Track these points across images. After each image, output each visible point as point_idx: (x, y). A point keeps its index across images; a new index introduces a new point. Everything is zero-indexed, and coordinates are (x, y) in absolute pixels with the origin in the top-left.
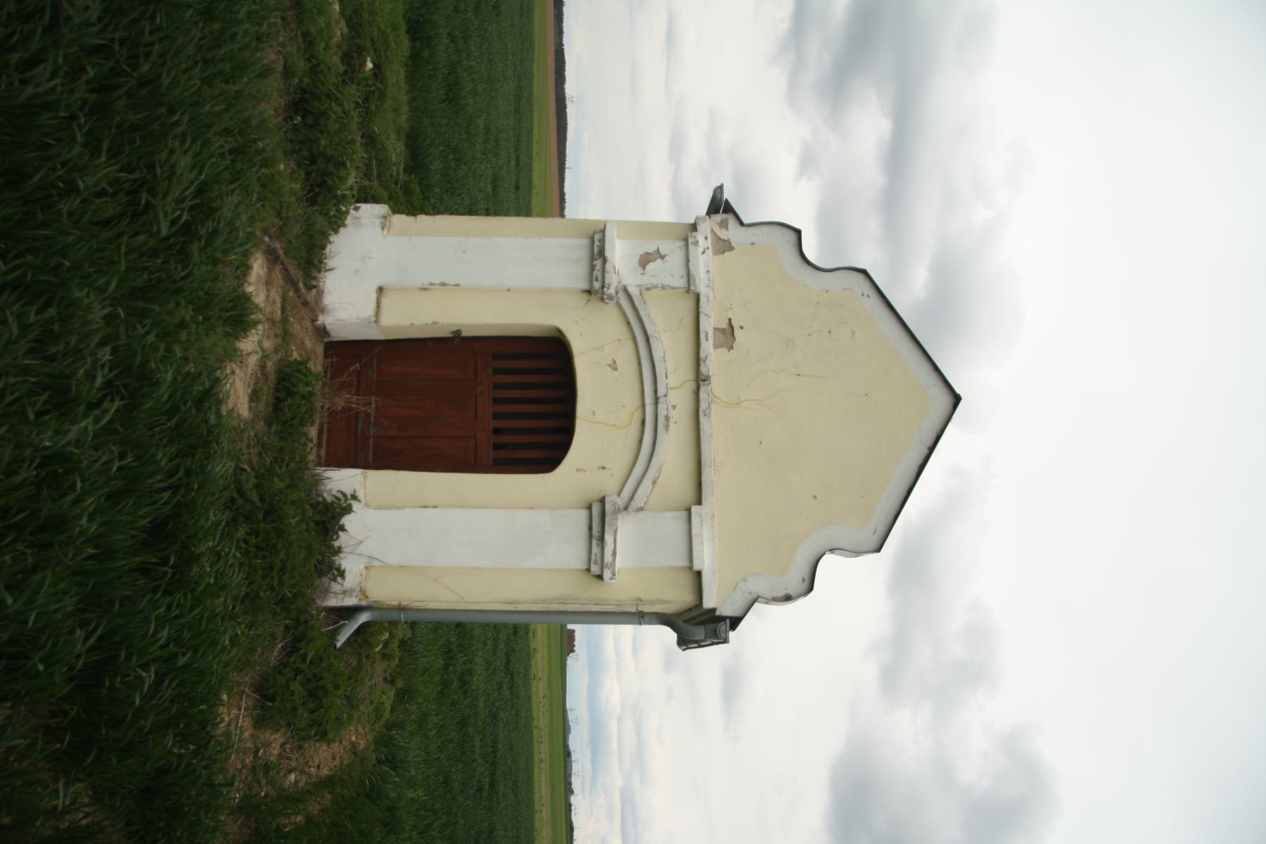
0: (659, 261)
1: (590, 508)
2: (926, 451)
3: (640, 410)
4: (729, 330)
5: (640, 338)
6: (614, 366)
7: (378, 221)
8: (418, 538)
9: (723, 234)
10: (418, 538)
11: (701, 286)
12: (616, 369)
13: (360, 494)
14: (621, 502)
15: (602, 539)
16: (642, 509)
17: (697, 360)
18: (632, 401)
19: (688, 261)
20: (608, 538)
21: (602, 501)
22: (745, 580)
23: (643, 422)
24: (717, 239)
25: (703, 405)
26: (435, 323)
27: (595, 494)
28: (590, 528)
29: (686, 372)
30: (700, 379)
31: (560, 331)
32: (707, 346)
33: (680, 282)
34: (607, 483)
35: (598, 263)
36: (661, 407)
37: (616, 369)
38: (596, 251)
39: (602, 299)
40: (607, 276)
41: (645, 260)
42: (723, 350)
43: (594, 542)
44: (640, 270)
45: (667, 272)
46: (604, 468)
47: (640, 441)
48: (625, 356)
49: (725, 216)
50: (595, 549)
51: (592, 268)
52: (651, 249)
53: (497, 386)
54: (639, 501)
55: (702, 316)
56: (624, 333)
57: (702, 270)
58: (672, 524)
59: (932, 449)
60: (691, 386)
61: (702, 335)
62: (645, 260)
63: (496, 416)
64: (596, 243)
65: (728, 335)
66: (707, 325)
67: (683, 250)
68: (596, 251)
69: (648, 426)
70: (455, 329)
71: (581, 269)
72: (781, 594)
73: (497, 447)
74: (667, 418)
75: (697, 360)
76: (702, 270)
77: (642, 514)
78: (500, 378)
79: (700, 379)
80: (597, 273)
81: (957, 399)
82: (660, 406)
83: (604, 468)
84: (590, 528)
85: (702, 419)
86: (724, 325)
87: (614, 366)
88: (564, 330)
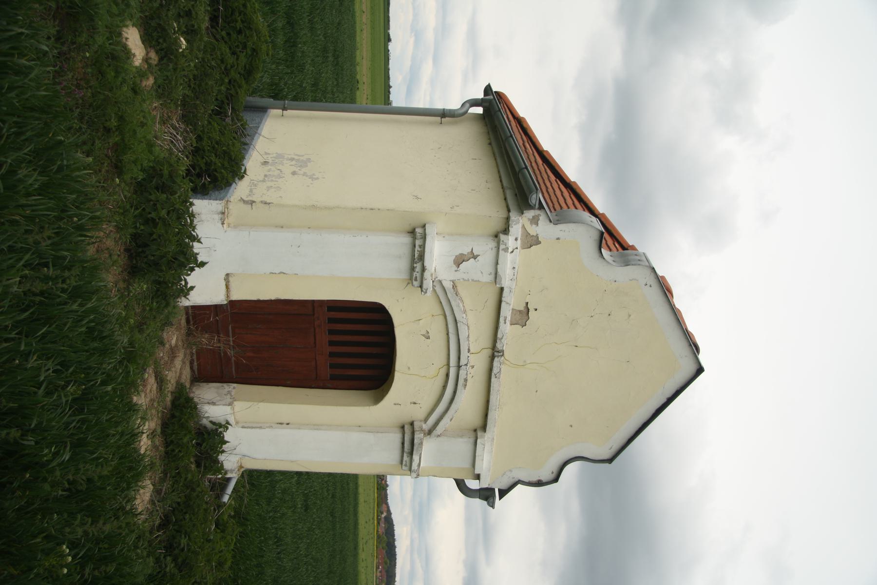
0: (472, 260)
1: (403, 427)
2: (664, 400)
3: (445, 368)
4: (526, 311)
5: (451, 324)
7: (217, 217)
8: (272, 432)
9: (532, 230)
10: (272, 432)
11: (506, 283)
12: (428, 338)
13: (232, 420)
14: (426, 427)
15: (411, 453)
16: (439, 436)
17: (495, 339)
18: (440, 360)
19: (497, 263)
20: (416, 457)
21: (412, 424)
22: (511, 471)
23: (447, 375)
24: (526, 234)
25: (495, 370)
27: (407, 419)
28: (403, 444)
29: (486, 342)
30: (495, 353)
32: (506, 328)
33: (488, 278)
34: (418, 413)
35: (418, 266)
36: (462, 373)
37: (428, 338)
38: (416, 255)
40: (425, 282)
41: (459, 261)
42: (534, 226)
43: (405, 455)
44: (455, 268)
45: (478, 270)
47: (445, 387)
48: (436, 328)
49: (537, 212)
50: (406, 458)
51: (413, 269)
52: (466, 251)
53: (331, 321)
54: (440, 429)
55: (503, 304)
56: (437, 310)
57: (509, 266)
58: (463, 445)
59: (670, 400)
60: (487, 352)
61: (502, 320)
62: (459, 261)
63: (331, 343)
64: (417, 248)
65: (523, 315)
66: (506, 312)
67: (495, 250)
68: (416, 255)
69: (451, 380)
71: (403, 264)
72: (534, 479)
73: (332, 366)
74: (466, 380)
75: (495, 339)
76: (509, 266)
77: (439, 439)
78: (333, 315)
79: (495, 353)
80: (417, 274)
81: (700, 370)
82: (461, 372)
84: (403, 444)
85: (493, 379)
86: (522, 307)
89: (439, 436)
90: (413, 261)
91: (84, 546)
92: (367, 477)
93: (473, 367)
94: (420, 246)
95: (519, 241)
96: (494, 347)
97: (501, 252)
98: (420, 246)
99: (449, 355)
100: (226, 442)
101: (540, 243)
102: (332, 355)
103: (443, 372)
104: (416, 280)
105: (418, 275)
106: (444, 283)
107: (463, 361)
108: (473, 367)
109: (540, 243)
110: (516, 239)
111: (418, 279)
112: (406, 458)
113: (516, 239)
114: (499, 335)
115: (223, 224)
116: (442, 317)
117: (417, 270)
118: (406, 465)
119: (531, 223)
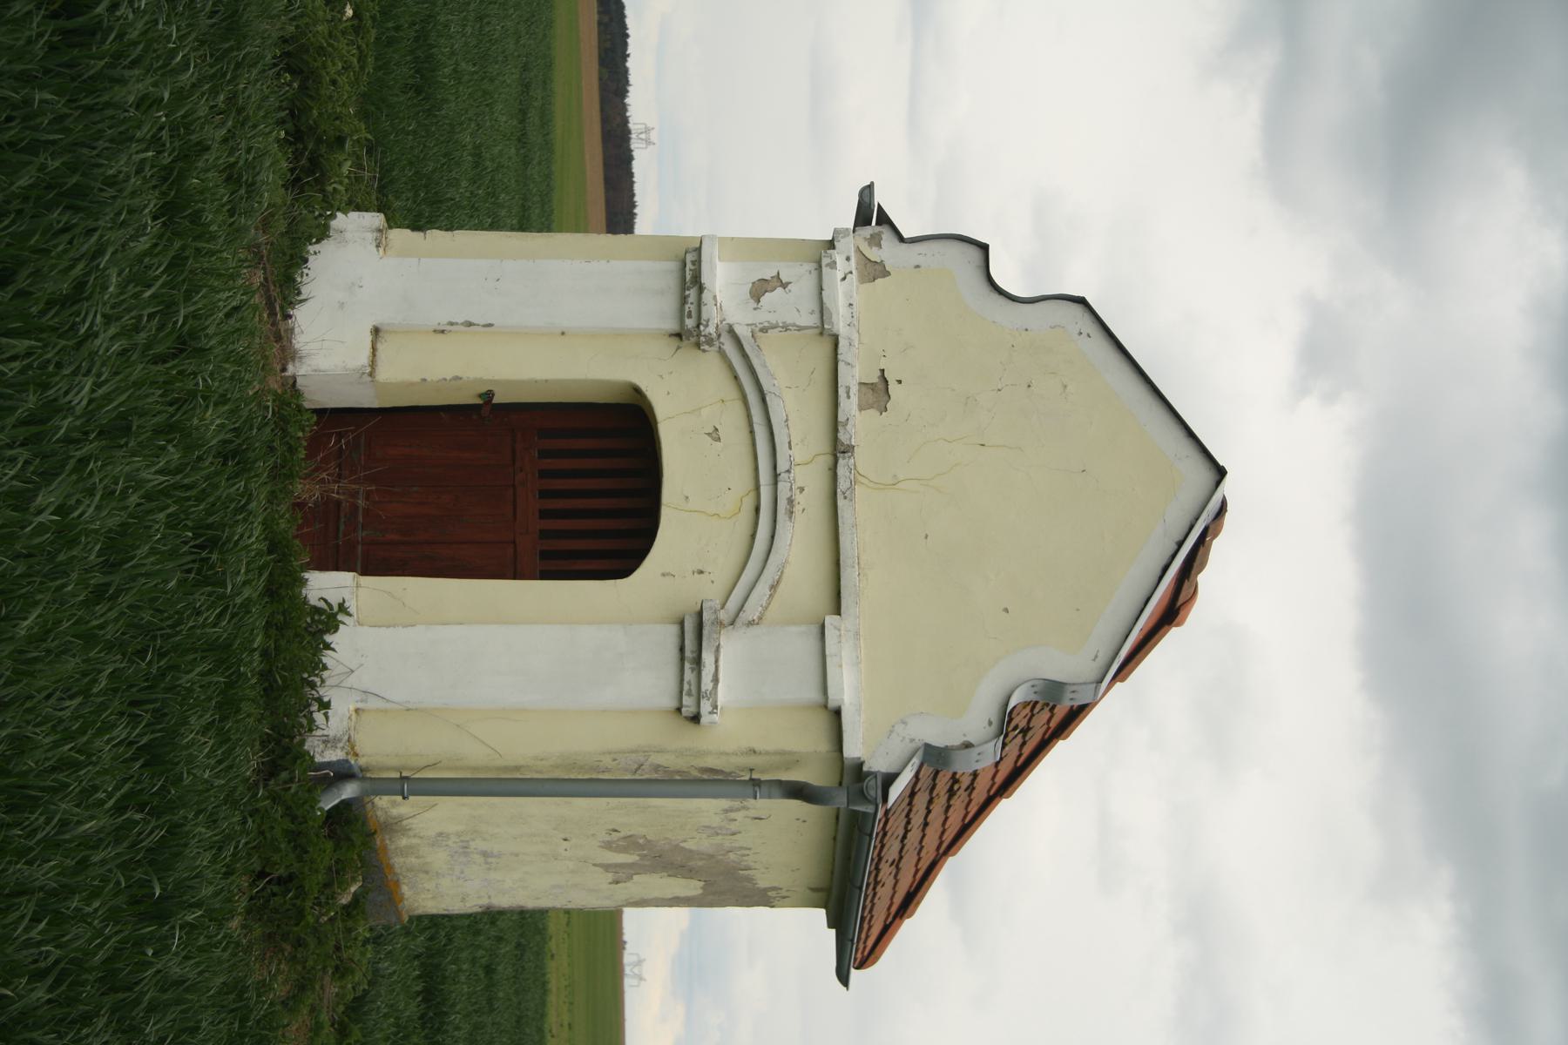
0: (780, 290)
1: (682, 623)
3: (752, 494)
4: (881, 386)
6: (715, 435)
7: (370, 236)
9: (873, 254)
11: (841, 326)
14: (724, 616)
16: (751, 623)
17: (835, 425)
22: (904, 723)
26: (457, 378)
30: (838, 449)
31: (637, 390)
32: (849, 406)
34: (709, 591)
35: (692, 293)
36: (783, 487)
38: (688, 277)
39: (698, 345)
40: (704, 309)
41: (759, 290)
43: (687, 666)
44: (753, 304)
46: (701, 572)
48: (731, 421)
50: (689, 675)
51: (684, 300)
52: (768, 274)
53: (544, 474)
55: (841, 366)
56: (730, 392)
57: (841, 302)
61: (841, 391)
62: (759, 290)
64: (689, 265)
65: (879, 391)
67: (815, 273)
68: (688, 277)
69: (765, 510)
70: (484, 390)
74: (791, 501)
75: (835, 425)
77: (754, 630)
79: (838, 449)
80: (690, 306)
82: (780, 485)
83: (701, 572)
84: (682, 649)
85: (841, 502)
86: (874, 378)
87: (715, 435)
88: (643, 389)
89: (751, 623)
90: (683, 286)
91: (111, 29)
92: (579, 226)
93: (802, 489)
94: (693, 263)
95: (853, 260)
96: (835, 440)
97: (825, 270)
98: (693, 263)
99: (756, 469)
100: (325, 668)
101: (889, 274)
102: (545, 534)
103: (749, 503)
104: (690, 316)
105: (693, 308)
106: (738, 330)
107: (782, 467)
108: (802, 489)
109: (889, 274)
110: (848, 259)
111: (694, 314)
112: (689, 675)
113: (848, 259)
114: (841, 418)
115: (378, 246)
116: (738, 405)
117: (691, 300)
118: (689, 694)
119: (870, 245)
